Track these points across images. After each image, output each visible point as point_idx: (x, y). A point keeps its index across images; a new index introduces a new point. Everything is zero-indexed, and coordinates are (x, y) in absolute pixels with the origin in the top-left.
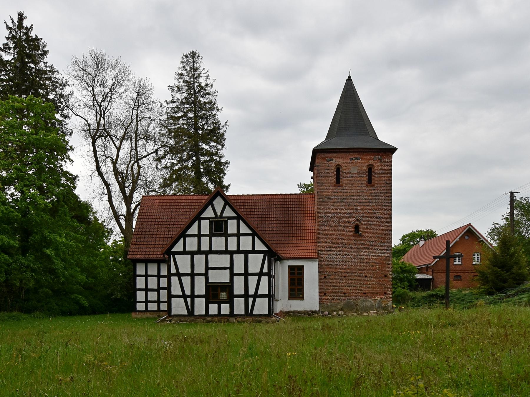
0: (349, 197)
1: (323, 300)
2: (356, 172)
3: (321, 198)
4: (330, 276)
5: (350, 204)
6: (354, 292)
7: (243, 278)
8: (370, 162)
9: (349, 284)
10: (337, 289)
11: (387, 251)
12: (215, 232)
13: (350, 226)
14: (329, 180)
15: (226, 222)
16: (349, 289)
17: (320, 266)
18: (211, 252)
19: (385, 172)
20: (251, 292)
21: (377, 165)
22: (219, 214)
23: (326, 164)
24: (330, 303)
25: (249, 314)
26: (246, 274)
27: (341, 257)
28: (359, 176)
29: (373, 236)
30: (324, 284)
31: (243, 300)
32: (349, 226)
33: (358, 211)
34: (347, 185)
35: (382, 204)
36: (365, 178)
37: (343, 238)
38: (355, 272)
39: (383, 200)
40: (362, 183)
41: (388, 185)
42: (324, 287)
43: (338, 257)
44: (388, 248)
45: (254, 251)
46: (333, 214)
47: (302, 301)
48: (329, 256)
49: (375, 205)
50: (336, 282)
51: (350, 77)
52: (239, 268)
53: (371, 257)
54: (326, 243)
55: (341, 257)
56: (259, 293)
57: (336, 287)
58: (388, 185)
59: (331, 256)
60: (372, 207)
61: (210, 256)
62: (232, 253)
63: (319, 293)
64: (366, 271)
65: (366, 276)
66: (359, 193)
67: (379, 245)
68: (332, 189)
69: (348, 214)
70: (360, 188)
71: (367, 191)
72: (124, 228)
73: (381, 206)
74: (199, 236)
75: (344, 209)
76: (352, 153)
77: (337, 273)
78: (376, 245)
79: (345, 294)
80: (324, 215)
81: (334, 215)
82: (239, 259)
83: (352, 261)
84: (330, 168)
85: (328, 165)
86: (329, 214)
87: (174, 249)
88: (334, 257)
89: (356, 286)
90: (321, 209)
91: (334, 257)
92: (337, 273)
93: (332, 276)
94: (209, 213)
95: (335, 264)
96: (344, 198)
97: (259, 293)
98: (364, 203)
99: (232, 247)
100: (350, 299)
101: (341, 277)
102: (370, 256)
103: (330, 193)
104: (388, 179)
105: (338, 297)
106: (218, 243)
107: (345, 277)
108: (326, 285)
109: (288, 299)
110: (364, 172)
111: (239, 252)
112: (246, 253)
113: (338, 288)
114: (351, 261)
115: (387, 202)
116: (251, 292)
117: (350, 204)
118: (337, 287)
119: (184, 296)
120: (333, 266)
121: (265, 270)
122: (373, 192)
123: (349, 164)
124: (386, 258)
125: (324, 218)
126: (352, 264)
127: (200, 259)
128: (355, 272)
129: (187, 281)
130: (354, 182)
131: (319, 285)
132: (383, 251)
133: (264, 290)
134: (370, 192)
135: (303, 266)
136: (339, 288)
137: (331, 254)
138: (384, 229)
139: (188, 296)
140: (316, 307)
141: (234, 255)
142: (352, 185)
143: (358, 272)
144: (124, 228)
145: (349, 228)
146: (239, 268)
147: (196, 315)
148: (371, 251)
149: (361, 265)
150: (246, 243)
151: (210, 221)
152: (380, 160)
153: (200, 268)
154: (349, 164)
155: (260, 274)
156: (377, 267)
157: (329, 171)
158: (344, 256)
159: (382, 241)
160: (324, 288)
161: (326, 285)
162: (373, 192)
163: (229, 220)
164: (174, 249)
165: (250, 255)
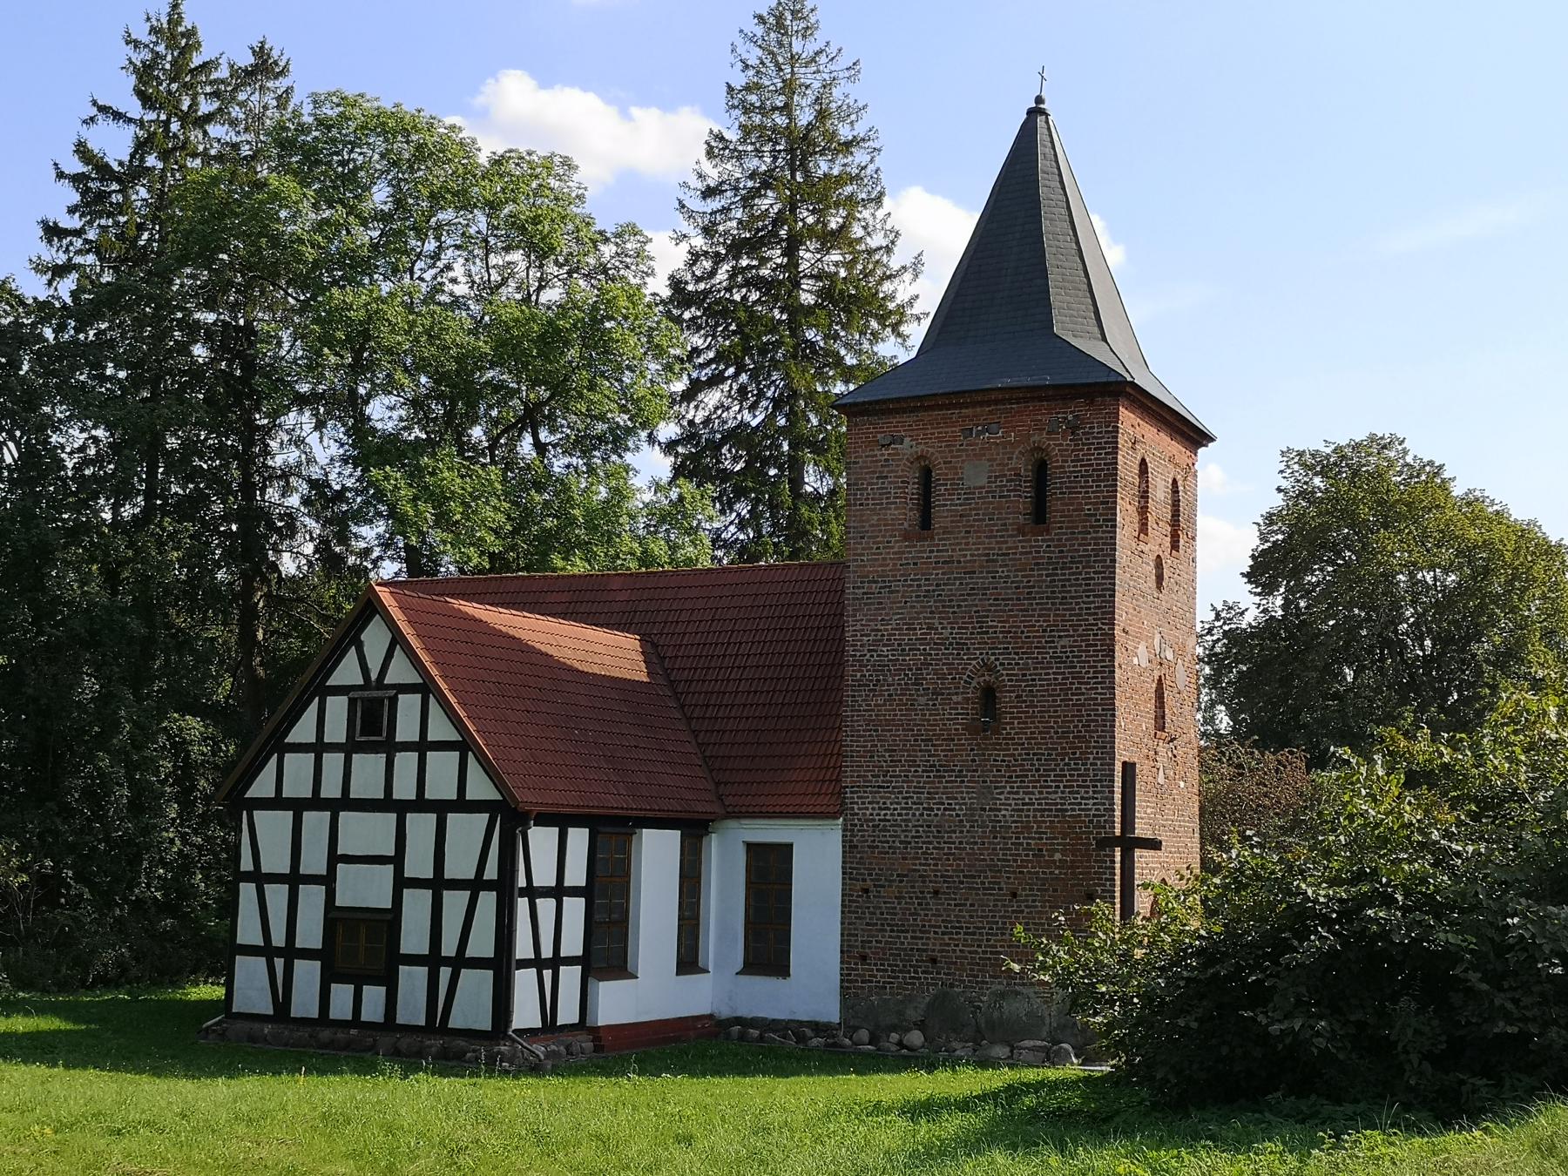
0: (955, 579)
1: (857, 981)
2: (983, 481)
3: (859, 588)
4: (883, 886)
5: (959, 606)
6: (966, 958)
7: (427, 894)
8: (1036, 438)
9: (951, 922)
10: (906, 940)
11: (1094, 792)
12: (362, 735)
13: (957, 694)
14: (889, 517)
15: (394, 701)
16: (949, 945)
17: (849, 848)
18: (346, 803)
19: (1090, 476)
20: (449, 948)
21: (1058, 446)
22: (374, 676)
23: (879, 458)
24: (877, 994)
25: (437, 1023)
26: (438, 884)
27: (922, 815)
28: (993, 497)
29: (1040, 733)
30: (860, 918)
31: (423, 971)
32: (953, 691)
33: (987, 633)
34: (949, 533)
35: (1078, 603)
36: (1023, 500)
37: (931, 740)
38: (974, 877)
39: (1081, 585)
40: (1005, 525)
41: (1101, 526)
42: (860, 932)
43: (914, 815)
44: (1100, 781)
45: (462, 804)
46: (899, 645)
47: (781, 980)
48: (880, 809)
49: (1050, 609)
50: (904, 914)
51: (1039, 100)
52: (419, 864)
53: (1035, 816)
54: (872, 757)
55: (922, 815)
56: (470, 953)
57: (903, 932)
58: (1101, 526)
59: (888, 809)
60: (1039, 616)
61: (343, 816)
62: (401, 809)
63: (842, 952)
64: (1014, 872)
65: (1014, 895)
66: (993, 561)
67: (1062, 770)
68: (896, 550)
69: (951, 644)
70: (997, 543)
71: (1021, 553)
72: (317, 698)
73: (1074, 609)
74: (319, 748)
75: (937, 625)
76: (967, 408)
77: (906, 876)
78: (1055, 770)
79: (934, 961)
80: (869, 651)
81: (903, 650)
82: (421, 827)
83: (961, 832)
84: (892, 471)
85: (886, 460)
86: (884, 645)
87: (252, 793)
88: (899, 815)
89: (974, 934)
90: (858, 627)
91: (899, 815)
92: (906, 876)
93: (890, 886)
94: (347, 672)
95: (901, 842)
96: (937, 585)
97: (470, 953)
98: (1012, 599)
99: (404, 789)
100: (952, 986)
101: (922, 892)
102: (1031, 814)
103: (890, 567)
104: (1102, 503)
105: (909, 972)
106: (368, 774)
107: (936, 893)
108: (867, 924)
109: (739, 965)
110: (1011, 480)
111: (420, 804)
112: (441, 809)
113: (909, 935)
114: (958, 829)
115: (1095, 596)
116: (449, 948)
117: (959, 606)
118: (908, 931)
119: (266, 951)
120: (895, 848)
121: (491, 872)
122: (1043, 557)
123: (958, 451)
124: (1091, 822)
125: (868, 661)
126: (961, 843)
127: (317, 822)
128: (974, 877)
129: (277, 895)
130: (974, 520)
131: (842, 923)
132: (1078, 793)
133: (482, 944)
134: (1034, 558)
135: (790, 846)
136: (912, 938)
137: (888, 802)
138: (1083, 705)
139: (279, 952)
140: (829, 1010)
141: (408, 815)
142: (967, 532)
143: (986, 877)
144: (317, 698)
145: (954, 698)
146: (419, 864)
147: (296, 1020)
148: (1033, 793)
149: (995, 849)
150: (442, 776)
151: (349, 699)
152: (1073, 429)
153: (314, 862)
154: (958, 451)
155: (475, 886)
156: (1058, 856)
157: (890, 483)
158: (932, 809)
159: (1074, 753)
160: (859, 932)
161: (867, 924)
162: (1043, 557)
163: (400, 696)
164: (252, 793)
165: (452, 818)
